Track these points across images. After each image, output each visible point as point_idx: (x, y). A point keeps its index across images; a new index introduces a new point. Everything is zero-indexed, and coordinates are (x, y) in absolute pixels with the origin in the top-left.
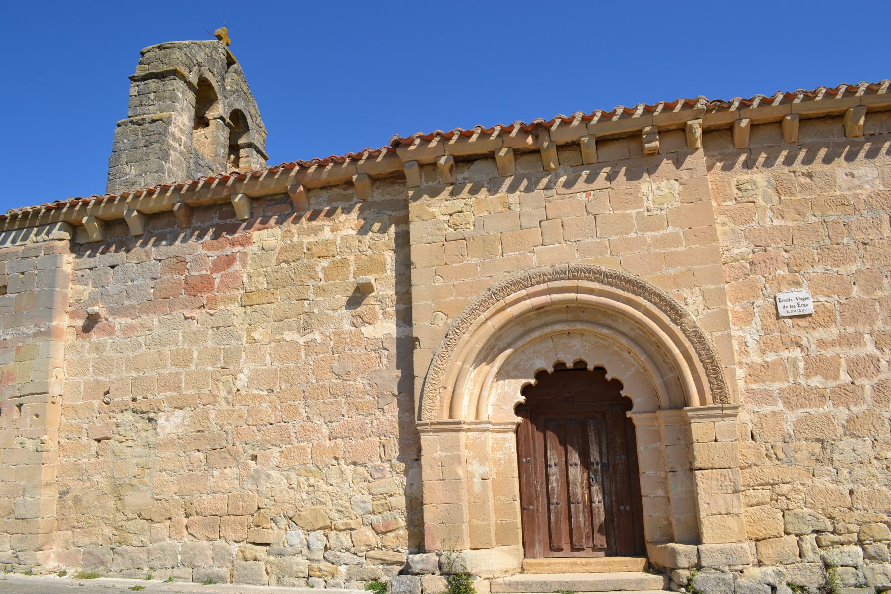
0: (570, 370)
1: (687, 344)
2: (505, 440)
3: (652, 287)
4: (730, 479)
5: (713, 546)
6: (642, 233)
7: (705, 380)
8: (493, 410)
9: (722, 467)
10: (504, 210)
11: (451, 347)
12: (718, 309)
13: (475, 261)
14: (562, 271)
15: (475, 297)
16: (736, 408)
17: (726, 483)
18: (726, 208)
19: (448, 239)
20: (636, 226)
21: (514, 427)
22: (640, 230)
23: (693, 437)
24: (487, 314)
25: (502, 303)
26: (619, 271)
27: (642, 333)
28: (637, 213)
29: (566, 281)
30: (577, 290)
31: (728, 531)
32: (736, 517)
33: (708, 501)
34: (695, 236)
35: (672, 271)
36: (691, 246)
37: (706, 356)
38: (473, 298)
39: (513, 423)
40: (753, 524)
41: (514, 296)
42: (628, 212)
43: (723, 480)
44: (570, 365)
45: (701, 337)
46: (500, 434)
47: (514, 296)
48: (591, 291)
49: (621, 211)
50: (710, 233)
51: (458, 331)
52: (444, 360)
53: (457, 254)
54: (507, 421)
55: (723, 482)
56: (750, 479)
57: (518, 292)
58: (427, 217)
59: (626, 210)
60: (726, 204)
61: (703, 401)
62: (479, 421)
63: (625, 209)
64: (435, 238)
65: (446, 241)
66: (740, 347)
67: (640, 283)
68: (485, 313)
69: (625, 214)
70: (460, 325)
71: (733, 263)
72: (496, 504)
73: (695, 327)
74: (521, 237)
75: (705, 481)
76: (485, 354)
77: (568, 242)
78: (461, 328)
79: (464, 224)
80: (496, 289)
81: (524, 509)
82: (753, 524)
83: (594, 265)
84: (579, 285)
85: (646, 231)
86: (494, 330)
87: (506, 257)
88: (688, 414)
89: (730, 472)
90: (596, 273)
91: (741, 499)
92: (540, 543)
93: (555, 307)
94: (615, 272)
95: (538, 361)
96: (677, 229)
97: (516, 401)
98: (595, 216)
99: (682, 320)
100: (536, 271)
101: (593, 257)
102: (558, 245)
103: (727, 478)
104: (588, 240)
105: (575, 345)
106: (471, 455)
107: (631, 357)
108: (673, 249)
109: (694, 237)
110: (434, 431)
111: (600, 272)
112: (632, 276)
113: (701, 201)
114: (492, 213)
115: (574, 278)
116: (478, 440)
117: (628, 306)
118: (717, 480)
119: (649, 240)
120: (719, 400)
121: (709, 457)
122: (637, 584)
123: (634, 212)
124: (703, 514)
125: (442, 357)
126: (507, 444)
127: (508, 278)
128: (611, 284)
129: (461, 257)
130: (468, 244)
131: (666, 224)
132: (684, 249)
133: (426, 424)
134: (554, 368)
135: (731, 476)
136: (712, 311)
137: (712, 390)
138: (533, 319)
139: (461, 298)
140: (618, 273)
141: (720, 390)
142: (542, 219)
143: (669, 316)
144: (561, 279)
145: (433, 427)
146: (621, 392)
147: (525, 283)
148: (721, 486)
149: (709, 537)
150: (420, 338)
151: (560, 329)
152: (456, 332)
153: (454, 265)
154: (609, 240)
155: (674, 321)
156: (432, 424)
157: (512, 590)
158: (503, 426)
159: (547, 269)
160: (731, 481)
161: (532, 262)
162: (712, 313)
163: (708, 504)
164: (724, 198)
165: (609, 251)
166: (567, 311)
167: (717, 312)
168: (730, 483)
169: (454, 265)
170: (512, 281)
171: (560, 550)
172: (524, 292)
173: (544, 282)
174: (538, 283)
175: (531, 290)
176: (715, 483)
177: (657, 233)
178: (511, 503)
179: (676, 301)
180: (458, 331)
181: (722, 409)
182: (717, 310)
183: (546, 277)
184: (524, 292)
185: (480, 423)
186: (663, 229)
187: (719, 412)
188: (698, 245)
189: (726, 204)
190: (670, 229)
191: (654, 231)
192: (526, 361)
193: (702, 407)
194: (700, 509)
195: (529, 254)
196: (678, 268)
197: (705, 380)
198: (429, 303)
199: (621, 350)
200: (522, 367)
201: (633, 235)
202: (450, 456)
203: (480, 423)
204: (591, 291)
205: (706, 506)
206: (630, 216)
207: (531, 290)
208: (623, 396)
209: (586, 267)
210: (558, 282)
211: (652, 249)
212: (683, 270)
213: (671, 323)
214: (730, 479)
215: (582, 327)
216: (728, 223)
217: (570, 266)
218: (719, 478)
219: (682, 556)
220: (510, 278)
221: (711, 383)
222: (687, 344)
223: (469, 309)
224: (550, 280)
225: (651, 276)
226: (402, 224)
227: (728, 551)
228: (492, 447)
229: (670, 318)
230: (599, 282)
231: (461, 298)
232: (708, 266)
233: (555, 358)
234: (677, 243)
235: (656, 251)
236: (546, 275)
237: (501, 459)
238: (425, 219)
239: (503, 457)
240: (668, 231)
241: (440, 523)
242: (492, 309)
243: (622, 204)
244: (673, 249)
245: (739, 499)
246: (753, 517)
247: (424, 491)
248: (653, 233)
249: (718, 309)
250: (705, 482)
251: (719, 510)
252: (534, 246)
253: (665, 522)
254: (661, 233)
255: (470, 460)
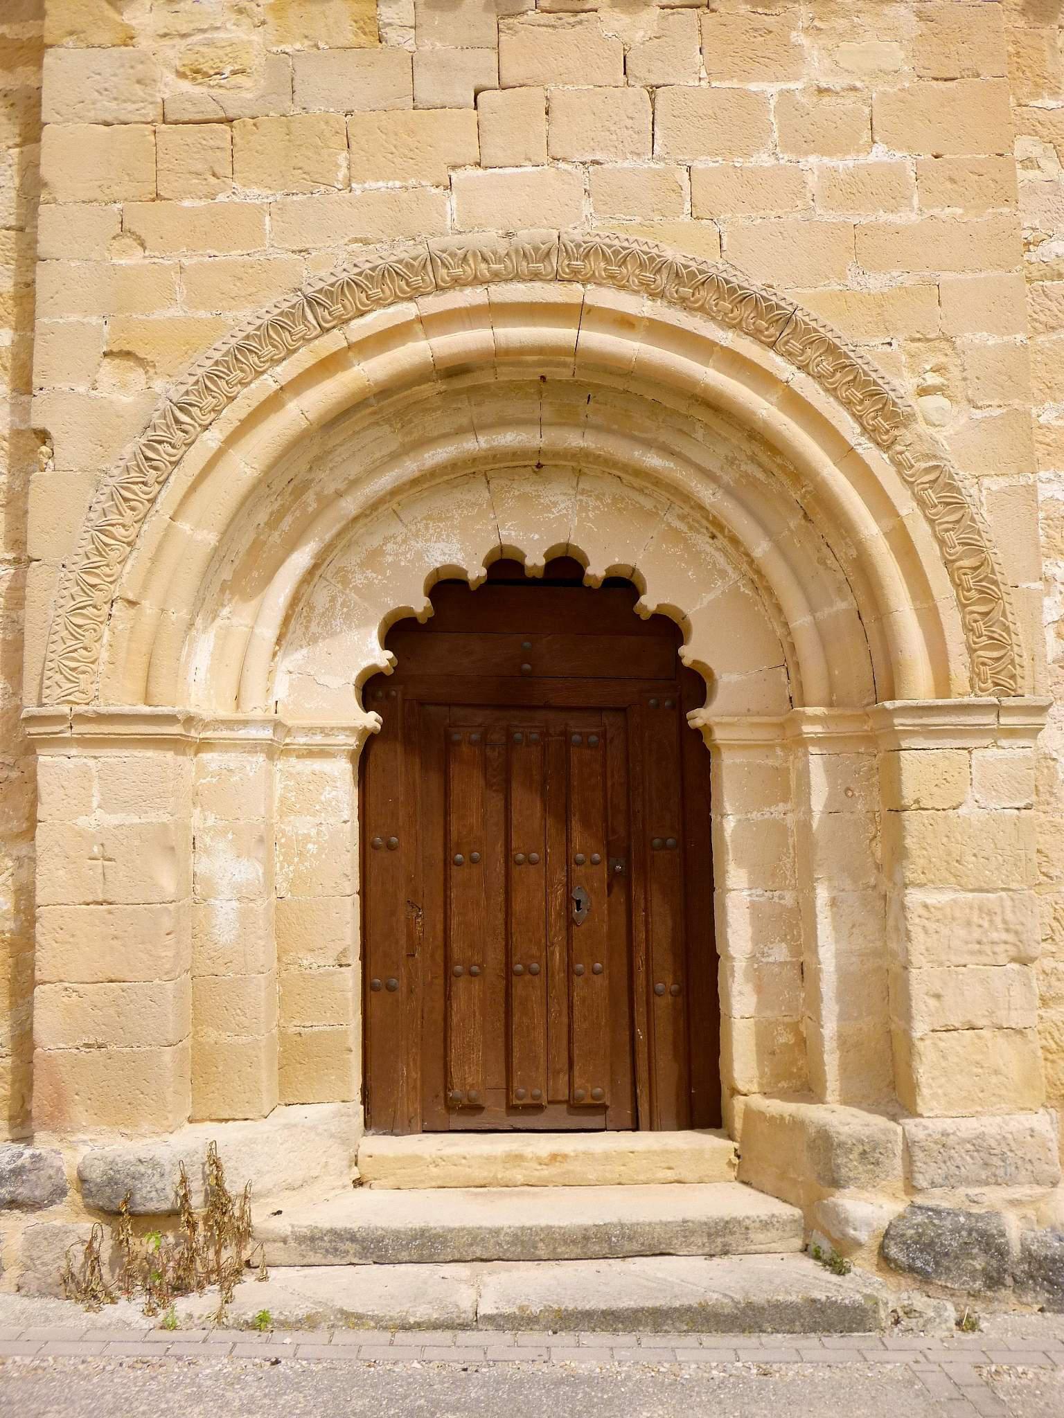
0: (534, 581)
1: (906, 506)
2: (320, 779)
3: (813, 324)
4: (1005, 922)
5: (948, 1124)
6: (794, 158)
7: (952, 620)
8: (291, 685)
9: (985, 886)
10: (363, 39)
11: (156, 468)
12: (1004, 410)
13: (255, 194)
14: (536, 249)
15: (248, 312)
16: (1042, 710)
17: (995, 936)
18: (1041, 115)
19: (170, 117)
20: (776, 135)
21: (353, 742)
22: (786, 148)
23: (905, 792)
24: (285, 371)
25: (334, 341)
26: (715, 264)
27: (760, 475)
28: (782, 93)
29: (547, 286)
30: (580, 313)
31: (994, 1079)
32: (1018, 1038)
33: (937, 987)
34: (952, 180)
35: (875, 283)
36: (936, 211)
37: (959, 548)
38: (240, 314)
39: (352, 729)
40: (1054, 1057)
41: (378, 320)
42: (753, 87)
43: (986, 924)
44: (535, 559)
45: (952, 487)
46: (308, 762)
47: (378, 320)
48: (625, 323)
49: (735, 84)
50: (998, 177)
51: (183, 417)
52: (133, 509)
53: (199, 167)
54: (333, 723)
55: (985, 932)
56: (1055, 924)
57: (392, 309)
58: (105, 37)
59: (749, 80)
60: (1039, 103)
61: (943, 683)
62: (240, 716)
63: (747, 75)
64: (126, 110)
65: (164, 122)
66: (1051, 532)
67: (778, 307)
68: (279, 369)
69: (747, 94)
70: (192, 398)
71: (1048, 283)
72: (284, 974)
73: (935, 457)
74: (412, 133)
75: (932, 926)
76: (276, 506)
77: (562, 165)
78: (194, 410)
79: (227, 72)
80: (320, 291)
81: (375, 988)
82: (1054, 1057)
83: (639, 242)
84: (588, 301)
85: (806, 153)
86: (304, 424)
87: (358, 192)
88: (897, 721)
89: (1008, 903)
90: (642, 265)
91: (1034, 983)
92: (415, 1063)
93: (506, 374)
94: (704, 267)
95: (441, 545)
96: (899, 154)
97: (365, 664)
98: (653, 89)
99: (896, 432)
100: (452, 241)
101: (638, 219)
102: (530, 169)
103: (998, 919)
104: (626, 164)
105: (555, 504)
106: (210, 822)
107: (718, 549)
108: (884, 217)
109: (949, 185)
110: (84, 742)
111: (656, 265)
112: (756, 285)
113: (978, 76)
114: (321, 45)
115: (575, 277)
116: (235, 779)
117: (733, 382)
118: (969, 923)
119: (812, 180)
120: (989, 684)
121: (949, 854)
122: (709, 1235)
123: (772, 88)
124: (920, 1028)
125: (126, 500)
126: (327, 794)
127: (360, 260)
128: (684, 304)
129: (213, 180)
130: (236, 140)
131: (866, 136)
132: (914, 218)
133: (60, 719)
134: (489, 570)
135: (1009, 916)
136: (986, 412)
137: (971, 651)
138: (434, 410)
139: (202, 314)
140: (713, 270)
141: (995, 654)
142: (485, 82)
143: (858, 418)
144: (535, 277)
145: (79, 729)
146: (682, 650)
147: (416, 280)
148: (979, 943)
149: (934, 1096)
150: (54, 433)
151: (515, 444)
152: (177, 421)
153: (187, 203)
154: (689, 169)
155: (870, 432)
156: (81, 718)
157: (312, 1259)
158: (318, 739)
159: (489, 238)
160: (1007, 930)
161: (443, 216)
162: (985, 420)
163: (938, 996)
164: (1036, 85)
165: (688, 206)
166: (540, 393)
167: (1001, 417)
168: (1005, 936)
169: (187, 203)
170: (373, 269)
171: (474, 1108)
172: (407, 311)
173: (477, 281)
174: (458, 283)
175: (433, 304)
176: (962, 933)
177: (844, 164)
178: (332, 974)
179: (882, 372)
180: (183, 417)
181: (998, 709)
182: (998, 411)
183: (483, 266)
184: (407, 311)
185: (245, 723)
186: (858, 152)
187: (989, 719)
188: (960, 211)
189: (1039, 103)
190: (879, 153)
191: (830, 154)
192: (404, 541)
193: (940, 702)
194: (914, 1011)
195: (434, 191)
196: (895, 274)
197: (952, 620)
198: (95, 320)
199: (691, 528)
200: (390, 559)
201: (763, 159)
202: (131, 826)
203: (245, 723)
204: (625, 323)
205: (932, 1002)
206: (760, 100)
207: (433, 304)
208: (686, 662)
209: (616, 242)
210: (521, 286)
211: (819, 211)
212: (909, 281)
213: (863, 440)
214: (1005, 922)
215: (582, 444)
216: (1042, 163)
217: (564, 238)
218: (975, 919)
219: (854, 1155)
220: (370, 257)
221: (968, 629)
222: (906, 506)
223: (225, 348)
224: (496, 278)
225: (812, 291)
226: (25, 64)
227: (994, 1144)
228: (283, 800)
229: (861, 425)
230: (653, 295)
231: (202, 314)
232: (983, 275)
233: (494, 537)
234: (896, 198)
235: (831, 217)
236: (485, 260)
237: (307, 838)
238: (96, 40)
239: (313, 832)
240: (872, 158)
241: (88, 1046)
242: (304, 358)
243: (737, 60)
244: (884, 217)
245: (1027, 985)
246: (1056, 1034)
247: (39, 938)
248: (826, 160)
249: (1004, 410)
250: (931, 931)
251: (969, 1017)
252: (454, 167)
253: (786, 1038)
254: (851, 164)
255: (208, 840)
